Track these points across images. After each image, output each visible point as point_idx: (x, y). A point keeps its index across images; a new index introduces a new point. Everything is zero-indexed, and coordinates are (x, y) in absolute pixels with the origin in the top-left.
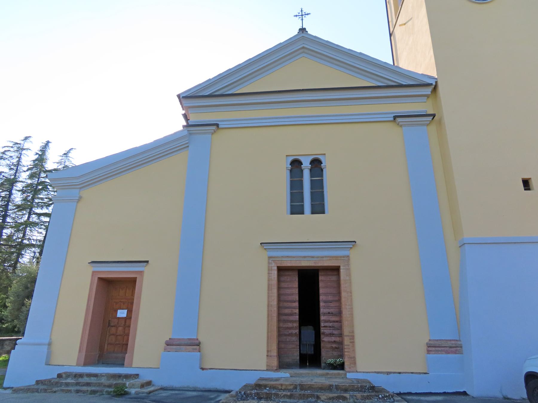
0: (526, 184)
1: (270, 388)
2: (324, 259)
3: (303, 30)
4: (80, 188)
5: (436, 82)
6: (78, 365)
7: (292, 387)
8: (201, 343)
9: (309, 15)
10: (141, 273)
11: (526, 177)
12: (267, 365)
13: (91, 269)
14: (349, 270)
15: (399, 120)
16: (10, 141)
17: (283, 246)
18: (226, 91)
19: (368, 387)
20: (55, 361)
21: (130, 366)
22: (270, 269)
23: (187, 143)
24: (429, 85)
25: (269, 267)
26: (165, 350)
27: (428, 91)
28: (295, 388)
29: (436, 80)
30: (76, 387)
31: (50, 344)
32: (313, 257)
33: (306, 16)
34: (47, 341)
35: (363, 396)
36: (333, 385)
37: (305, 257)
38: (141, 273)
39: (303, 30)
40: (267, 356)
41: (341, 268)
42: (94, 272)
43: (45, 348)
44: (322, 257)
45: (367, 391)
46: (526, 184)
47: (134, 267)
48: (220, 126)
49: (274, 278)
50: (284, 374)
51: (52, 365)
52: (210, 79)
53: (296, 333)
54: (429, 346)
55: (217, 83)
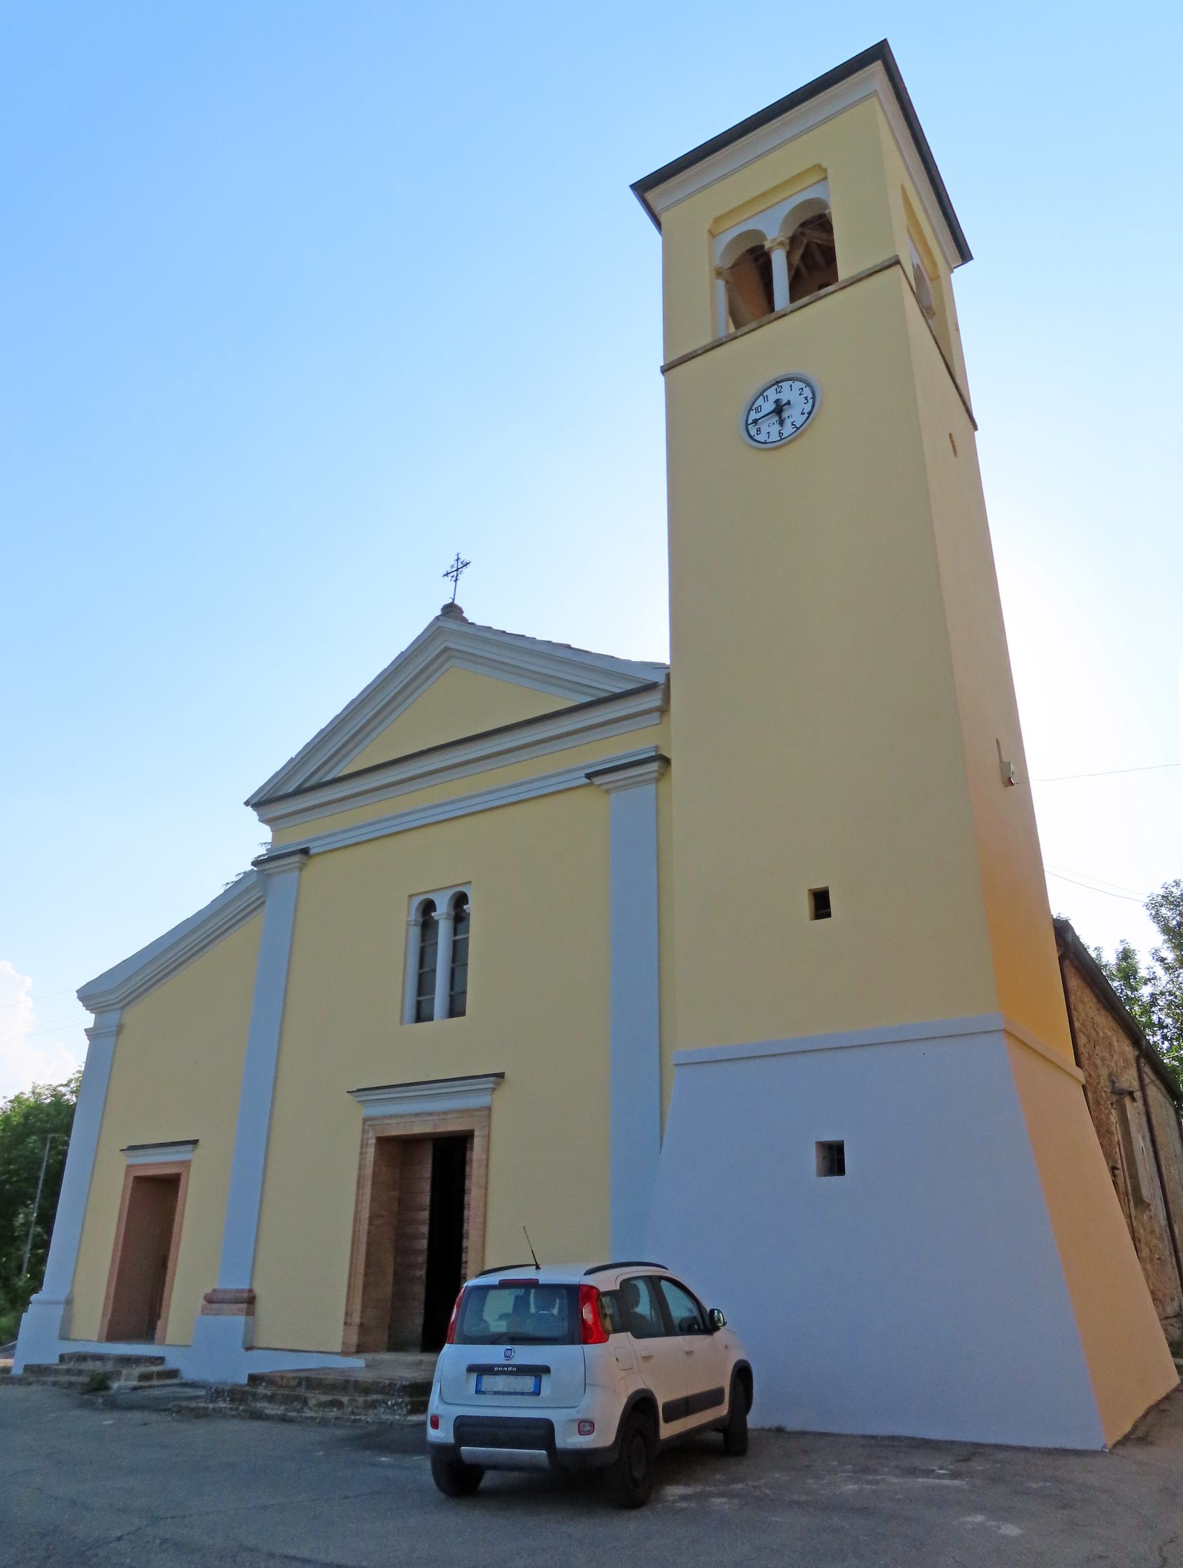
0: (821, 903)
1: (267, 1384)
2: (449, 1116)
3: (451, 611)
4: (123, 1008)
5: (668, 676)
6: (100, 1341)
7: (294, 1383)
8: (257, 1298)
9: (468, 565)
10: (187, 1164)
11: (819, 885)
12: (343, 1343)
13: (125, 1160)
14: (488, 1137)
15: (598, 780)
16: (266, 843)
17: (375, 1095)
18: (326, 774)
19: (398, 1385)
20: (263, 1340)
21: (162, 1342)
22: (364, 1145)
23: (261, 897)
24: (649, 687)
25: (363, 1139)
26: (204, 1311)
27: (653, 700)
28: (299, 1384)
29: (666, 671)
30: (230, 1388)
31: (69, 1302)
32: (430, 1114)
33: (464, 569)
34: (63, 1297)
35: (365, 1402)
36: (350, 1381)
37: (417, 1115)
38: (187, 1164)
39: (451, 611)
40: (345, 1323)
41: (476, 1134)
42: (129, 1168)
43: (59, 1310)
44: (445, 1113)
45: (396, 1393)
46: (821, 903)
47: (177, 1152)
48: (312, 852)
49: (370, 1161)
50: (358, 1362)
51: (260, 1348)
52: (292, 758)
53: (420, 1277)
54: (210, 1300)
55: (301, 766)
